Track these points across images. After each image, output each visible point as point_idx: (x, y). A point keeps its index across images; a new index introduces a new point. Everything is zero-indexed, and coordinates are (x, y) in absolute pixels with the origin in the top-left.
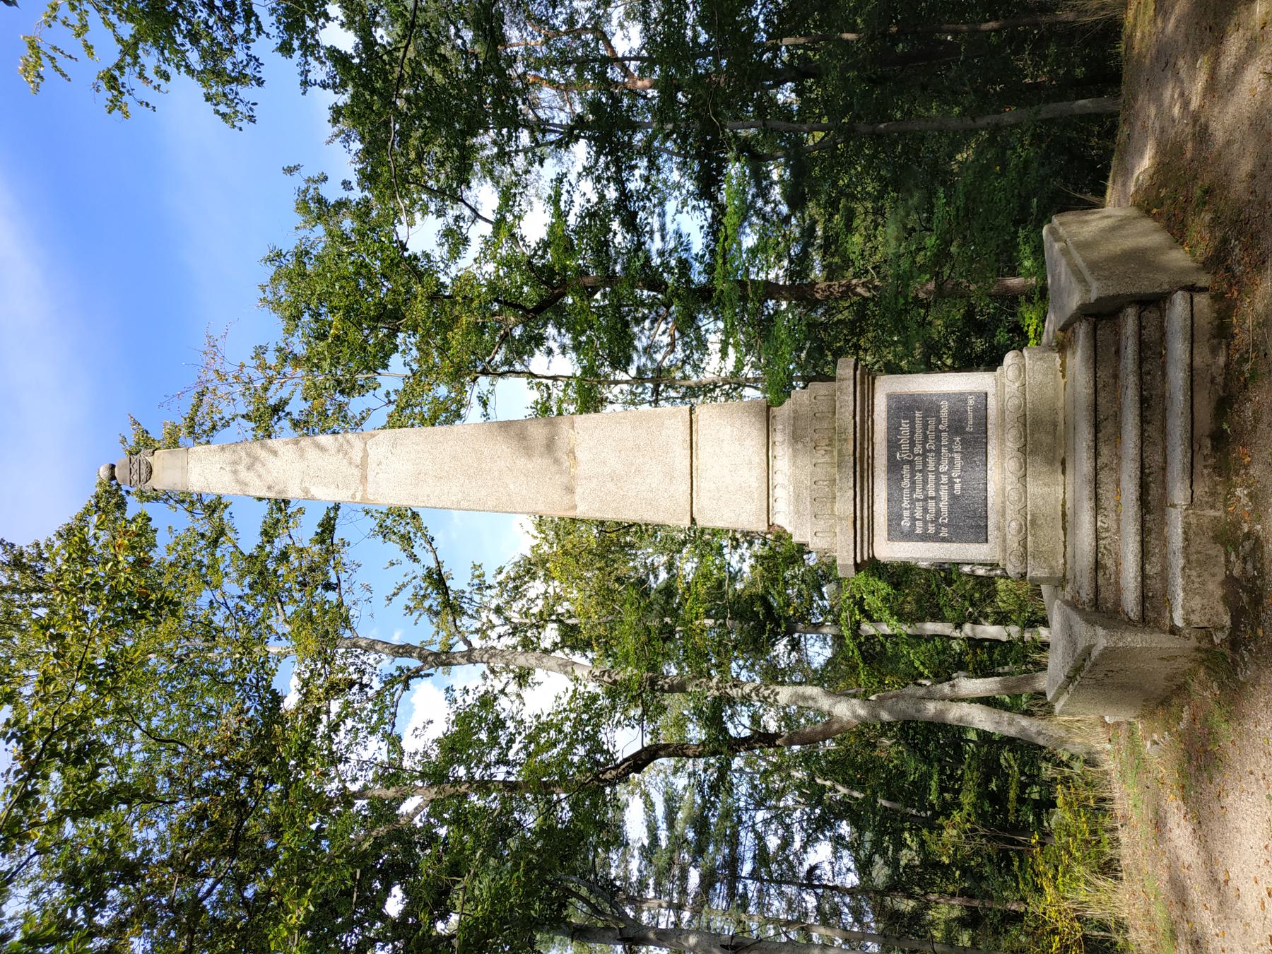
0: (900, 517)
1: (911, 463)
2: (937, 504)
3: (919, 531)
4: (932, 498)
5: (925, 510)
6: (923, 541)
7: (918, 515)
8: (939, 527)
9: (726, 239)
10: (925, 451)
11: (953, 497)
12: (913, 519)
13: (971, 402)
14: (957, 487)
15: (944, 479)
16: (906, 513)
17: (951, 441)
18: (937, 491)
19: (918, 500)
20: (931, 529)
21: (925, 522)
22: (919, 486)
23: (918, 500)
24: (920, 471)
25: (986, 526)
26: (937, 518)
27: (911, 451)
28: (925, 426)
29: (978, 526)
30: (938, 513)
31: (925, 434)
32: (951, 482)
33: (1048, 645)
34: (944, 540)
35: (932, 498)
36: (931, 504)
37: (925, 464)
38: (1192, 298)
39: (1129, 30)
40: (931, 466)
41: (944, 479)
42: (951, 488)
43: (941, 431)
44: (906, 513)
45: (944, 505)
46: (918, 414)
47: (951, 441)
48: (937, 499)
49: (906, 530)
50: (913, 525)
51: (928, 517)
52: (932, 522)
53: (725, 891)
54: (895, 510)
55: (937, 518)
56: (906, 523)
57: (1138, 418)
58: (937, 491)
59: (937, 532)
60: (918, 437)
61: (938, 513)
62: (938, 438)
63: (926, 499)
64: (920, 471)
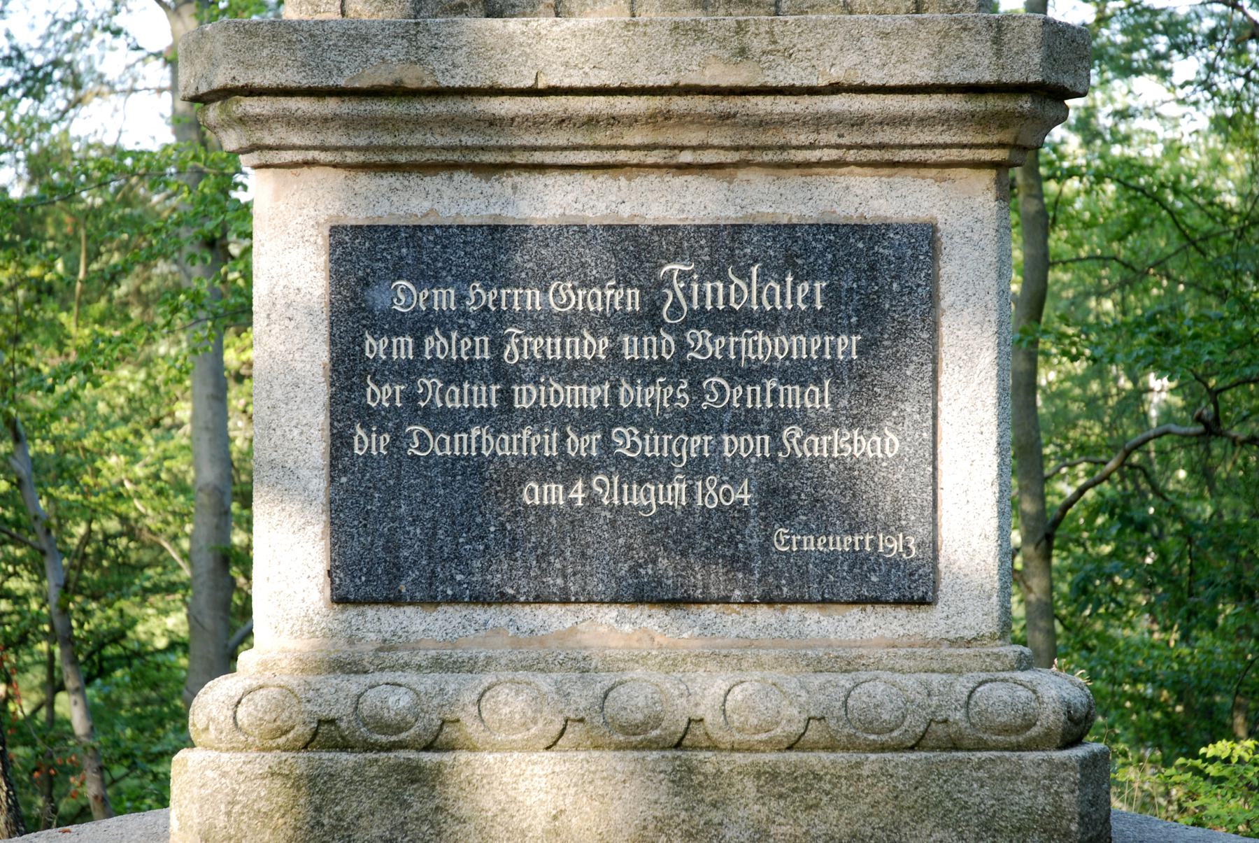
3: (375, 347)
5: (456, 372)
12: (420, 325)
15: (583, 445)
16: (444, 298)
18: (536, 417)
21: (407, 372)
27: (700, 318)
30: (454, 422)
36: (485, 395)
37: (644, 372)
41: (583, 445)
44: (444, 298)
47: (733, 471)
50: (394, 324)
56: (404, 295)
58: (536, 417)
59: (369, 417)
60: (757, 346)
61: (454, 422)
62: (746, 422)
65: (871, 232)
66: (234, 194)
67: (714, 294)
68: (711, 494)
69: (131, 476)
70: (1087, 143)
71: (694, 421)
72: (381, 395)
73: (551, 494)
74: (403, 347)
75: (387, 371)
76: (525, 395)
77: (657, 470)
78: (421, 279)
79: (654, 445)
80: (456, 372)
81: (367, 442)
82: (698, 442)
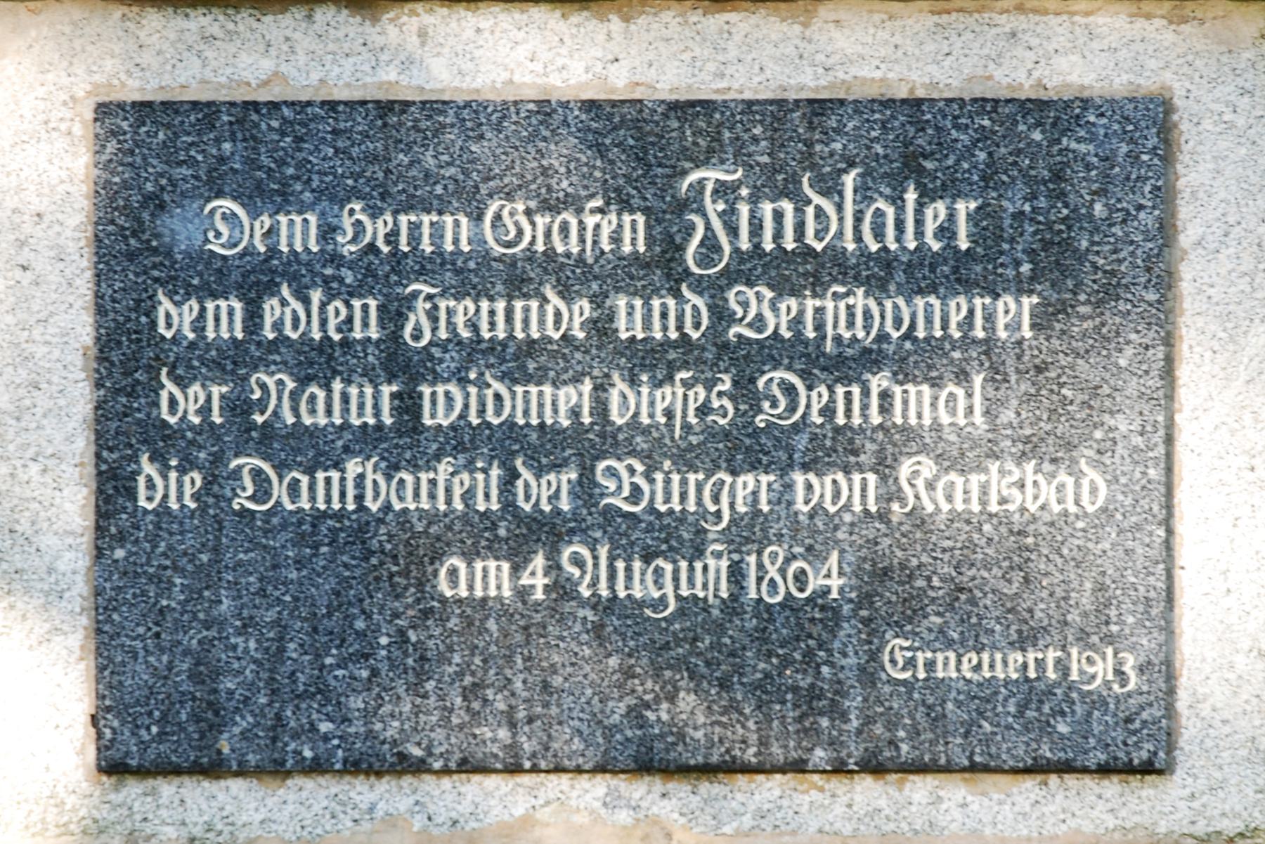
0: (267, 193)
1: (662, 267)
2: (368, 439)
3: (175, 317)
4: (408, 405)
5: (319, 362)
6: (105, 345)
7: (278, 311)
10: (746, 361)
11: (420, 545)
12: (256, 278)
13: (1096, 670)
14: (492, 578)
15: (547, 490)
16: (297, 232)
18: (463, 441)
19: (394, 314)
20: (187, 402)
21: (233, 361)
23: (394, 314)
24: (601, 327)
25: (213, 769)
26: (267, 440)
27: (754, 266)
29: (213, 717)
30: (313, 450)
31: (871, 358)
32: (530, 534)
34: (113, 487)
35: (408, 405)
36: (371, 403)
37: (650, 360)
40: (631, 402)
41: (547, 490)
43: (884, 466)
44: (297, 232)
45: (358, 482)
48: (403, 442)
49: (180, 229)
50: (208, 277)
51: (273, 384)
52: (239, 408)
54: (322, 156)
55: (267, 440)
56: (227, 226)
57: (873, 92)
58: (463, 441)
59: (165, 442)
61: (313, 450)
63: (403, 366)
64: (601, 327)
65: (1057, 114)
67: (778, 222)
68: (773, 576)
72: (187, 402)
75: (208, 277)
79: (673, 492)
81: (163, 487)
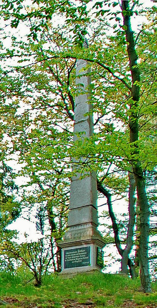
5: (69, 257)
8: (67, 259)
9: (122, 275)
12: (68, 255)
15: (75, 259)
16: (69, 253)
17: (81, 260)
18: (73, 258)
22: (73, 255)
27: (80, 253)
28: (84, 255)
33: (97, 9)
37: (77, 256)
38: (105, 204)
39: (130, 9)
41: (75, 259)
42: (73, 261)
46: (86, 253)
47: (81, 260)
50: (66, 255)
53: (20, 91)
58: (73, 258)
60: (82, 254)
62: (82, 257)
66: (115, 130)
69: (122, 109)
70: (44, 134)
71: (79, 258)
73: (73, 262)
74: (67, 256)
76: (72, 257)
77: (78, 260)
78: (68, 252)
80: (69, 257)
82: (80, 259)
